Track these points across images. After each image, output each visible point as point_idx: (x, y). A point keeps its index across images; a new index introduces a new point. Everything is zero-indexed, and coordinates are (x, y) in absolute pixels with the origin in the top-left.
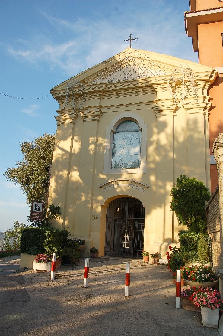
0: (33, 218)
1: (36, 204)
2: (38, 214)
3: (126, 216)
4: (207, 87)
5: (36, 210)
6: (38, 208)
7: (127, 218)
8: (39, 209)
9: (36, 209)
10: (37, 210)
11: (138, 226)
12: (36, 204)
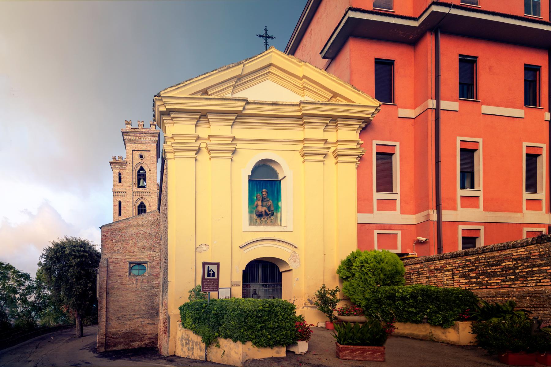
0: (206, 288)
1: (209, 267)
3: (529, 102)
5: (210, 277)
6: (211, 272)
8: (213, 275)
9: (209, 275)
10: (211, 276)
12: (209, 267)
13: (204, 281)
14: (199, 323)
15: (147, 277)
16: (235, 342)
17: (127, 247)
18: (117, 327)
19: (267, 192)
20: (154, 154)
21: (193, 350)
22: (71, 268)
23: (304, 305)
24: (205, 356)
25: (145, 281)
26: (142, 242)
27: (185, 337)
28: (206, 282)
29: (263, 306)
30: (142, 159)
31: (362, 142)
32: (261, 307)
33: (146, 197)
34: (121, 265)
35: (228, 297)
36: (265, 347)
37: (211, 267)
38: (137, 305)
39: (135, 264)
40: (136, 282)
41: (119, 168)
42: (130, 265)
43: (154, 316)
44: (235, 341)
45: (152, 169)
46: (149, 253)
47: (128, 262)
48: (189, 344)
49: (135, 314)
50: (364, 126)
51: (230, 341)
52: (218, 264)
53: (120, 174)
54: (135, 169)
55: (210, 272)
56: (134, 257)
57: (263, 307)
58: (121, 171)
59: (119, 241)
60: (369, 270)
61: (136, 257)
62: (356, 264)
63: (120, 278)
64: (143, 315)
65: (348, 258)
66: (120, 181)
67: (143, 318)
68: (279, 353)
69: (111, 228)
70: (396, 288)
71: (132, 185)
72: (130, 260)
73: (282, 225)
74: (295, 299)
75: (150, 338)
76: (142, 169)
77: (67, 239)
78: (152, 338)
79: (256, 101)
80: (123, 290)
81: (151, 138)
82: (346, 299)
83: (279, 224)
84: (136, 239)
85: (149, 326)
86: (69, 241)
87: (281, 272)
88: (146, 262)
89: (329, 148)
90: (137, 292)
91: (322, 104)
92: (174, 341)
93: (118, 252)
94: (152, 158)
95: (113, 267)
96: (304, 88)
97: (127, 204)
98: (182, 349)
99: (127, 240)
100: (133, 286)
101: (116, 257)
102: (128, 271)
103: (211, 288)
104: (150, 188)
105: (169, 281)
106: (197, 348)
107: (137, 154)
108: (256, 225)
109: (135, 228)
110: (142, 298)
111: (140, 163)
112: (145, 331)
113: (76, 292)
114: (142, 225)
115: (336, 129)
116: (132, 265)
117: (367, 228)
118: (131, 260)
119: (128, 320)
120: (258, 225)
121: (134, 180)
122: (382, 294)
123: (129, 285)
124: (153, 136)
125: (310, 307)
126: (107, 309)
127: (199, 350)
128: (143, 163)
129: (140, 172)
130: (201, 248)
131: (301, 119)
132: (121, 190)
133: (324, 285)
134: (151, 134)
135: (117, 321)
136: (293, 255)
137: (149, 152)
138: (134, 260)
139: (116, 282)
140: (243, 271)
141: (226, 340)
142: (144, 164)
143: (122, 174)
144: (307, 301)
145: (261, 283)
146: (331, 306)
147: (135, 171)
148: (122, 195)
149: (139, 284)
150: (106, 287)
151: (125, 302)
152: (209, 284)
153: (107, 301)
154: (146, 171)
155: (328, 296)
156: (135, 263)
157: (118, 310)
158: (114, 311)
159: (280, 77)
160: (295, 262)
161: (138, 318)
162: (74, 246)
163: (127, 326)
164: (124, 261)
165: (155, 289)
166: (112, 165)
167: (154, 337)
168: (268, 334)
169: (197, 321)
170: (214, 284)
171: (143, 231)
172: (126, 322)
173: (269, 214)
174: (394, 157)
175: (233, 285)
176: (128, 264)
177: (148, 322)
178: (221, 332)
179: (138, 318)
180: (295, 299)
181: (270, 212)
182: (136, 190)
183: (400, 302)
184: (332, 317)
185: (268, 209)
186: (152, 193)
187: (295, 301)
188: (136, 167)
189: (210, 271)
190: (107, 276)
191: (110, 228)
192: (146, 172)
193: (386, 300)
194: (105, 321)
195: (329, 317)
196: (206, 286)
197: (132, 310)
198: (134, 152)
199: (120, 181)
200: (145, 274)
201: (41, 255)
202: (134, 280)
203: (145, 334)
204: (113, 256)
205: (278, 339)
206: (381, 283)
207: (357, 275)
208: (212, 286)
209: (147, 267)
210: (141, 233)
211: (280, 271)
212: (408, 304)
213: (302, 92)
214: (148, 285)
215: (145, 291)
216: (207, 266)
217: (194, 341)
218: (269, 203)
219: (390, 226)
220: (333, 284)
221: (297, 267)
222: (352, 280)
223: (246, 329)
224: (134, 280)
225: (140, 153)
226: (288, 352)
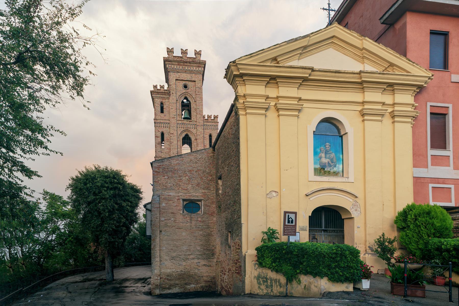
0: (286, 233)
1: (288, 216)
5: (290, 223)
7: (323, 228)
8: (292, 222)
9: (289, 222)
12: (288, 216)
13: (285, 227)
14: (279, 262)
15: (202, 215)
16: (315, 278)
17: (180, 184)
18: (172, 267)
19: (330, 146)
21: (272, 288)
22: (103, 201)
23: (364, 252)
24: (286, 292)
25: (199, 219)
26: (195, 179)
27: (262, 275)
28: (287, 228)
29: (336, 249)
30: (186, 89)
31: (417, 105)
32: (335, 251)
33: (191, 130)
34: (174, 202)
35: (297, 241)
36: (337, 282)
38: (192, 244)
39: (188, 202)
40: (191, 220)
42: (183, 203)
43: (210, 257)
44: (314, 277)
45: (198, 100)
46: (203, 191)
48: (267, 282)
49: (190, 255)
50: (419, 91)
51: (310, 277)
52: (295, 213)
57: (337, 251)
58: (164, 101)
59: (172, 177)
60: (422, 224)
61: (190, 195)
62: (413, 213)
63: (173, 216)
64: (199, 256)
65: (404, 209)
66: (162, 111)
67: (198, 259)
68: (348, 288)
69: (163, 164)
70: (443, 240)
71: (176, 116)
72: (183, 198)
73: (344, 176)
75: (206, 281)
77: (96, 168)
78: (209, 281)
79: (321, 69)
80: (177, 228)
81: (196, 68)
82: (402, 248)
83: (342, 175)
85: (204, 267)
86: (99, 171)
87: (343, 219)
88: (200, 201)
89: (387, 110)
90: (192, 231)
91: (379, 74)
93: (171, 189)
95: (166, 203)
96: (364, 57)
98: (259, 287)
100: (188, 224)
101: (168, 194)
102: (182, 208)
103: (291, 233)
104: (196, 120)
106: (277, 285)
107: (181, 84)
108: (320, 175)
109: (188, 165)
110: (197, 238)
111: (185, 93)
112: (201, 272)
113: (108, 228)
114: (196, 163)
115: (393, 92)
117: (423, 181)
118: (185, 198)
119: (183, 260)
120: (322, 175)
122: (431, 246)
123: (183, 223)
124: (199, 67)
125: (371, 254)
127: (279, 287)
128: (188, 94)
131: (361, 84)
132: (164, 121)
133: (383, 233)
134: (196, 64)
135: (172, 261)
137: (194, 83)
138: (188, 198)
140: (309, 216)
141: (306, 276)
142: (189, 94)
143: (164, 104)
144: (368, 248)
146: (390, 254)
149: (194, 223)
150: (159, 224)
151: (179, 241)
154: (191, 102)
155: (387, 244)
156: (189, 200)
157: (172, 249)
158: (168, 250)
159: (342, 46)
161: (193, 259)
162: (106, 177)
163: (183, 267)
164: (177, 199)
165: (211, 228)
166: (153, 94)
167: (210, 280)
168: (340, 272)
169: (278, 260)
170: (293, 229)
171: (196, 168)
174: (447, 116)
176: (182, 202)
177: (204, 263)
178: (302, 269)
179: (193, 259)
180: (357, 245)
182: (180, 122)
183: (446, 253)
184: (391, 264)
185: (331, 161)
186: (198, 126)
189: (290, 219)
191: (161, 164)
192: (190, 103)
193: (435, 251)
194: (159, 260)
195: (388, 264)
196: (287, 231)
197: (187, 249)
198: (177, 81)
199: (162, 111)
200: (199, 213)
201: (67, 186)
202: (188, 218)
203: (201, 276)
204: (166, 193)
206: (432, 236)
207: (411, 226)
209: (202, 205)
211: (342, 218)
212: (452, 255)
213: (362, 60)
214: (203, 224)
215: (200, 231)
216: (287, 214)
217: (273, 279)
218: (332, 156)
219: (444, 181)
220: (392, 234)
222: (408, 230)
223: (323, 267)
224: (188, 218)
225: (184, 82)
226: (354, 288)
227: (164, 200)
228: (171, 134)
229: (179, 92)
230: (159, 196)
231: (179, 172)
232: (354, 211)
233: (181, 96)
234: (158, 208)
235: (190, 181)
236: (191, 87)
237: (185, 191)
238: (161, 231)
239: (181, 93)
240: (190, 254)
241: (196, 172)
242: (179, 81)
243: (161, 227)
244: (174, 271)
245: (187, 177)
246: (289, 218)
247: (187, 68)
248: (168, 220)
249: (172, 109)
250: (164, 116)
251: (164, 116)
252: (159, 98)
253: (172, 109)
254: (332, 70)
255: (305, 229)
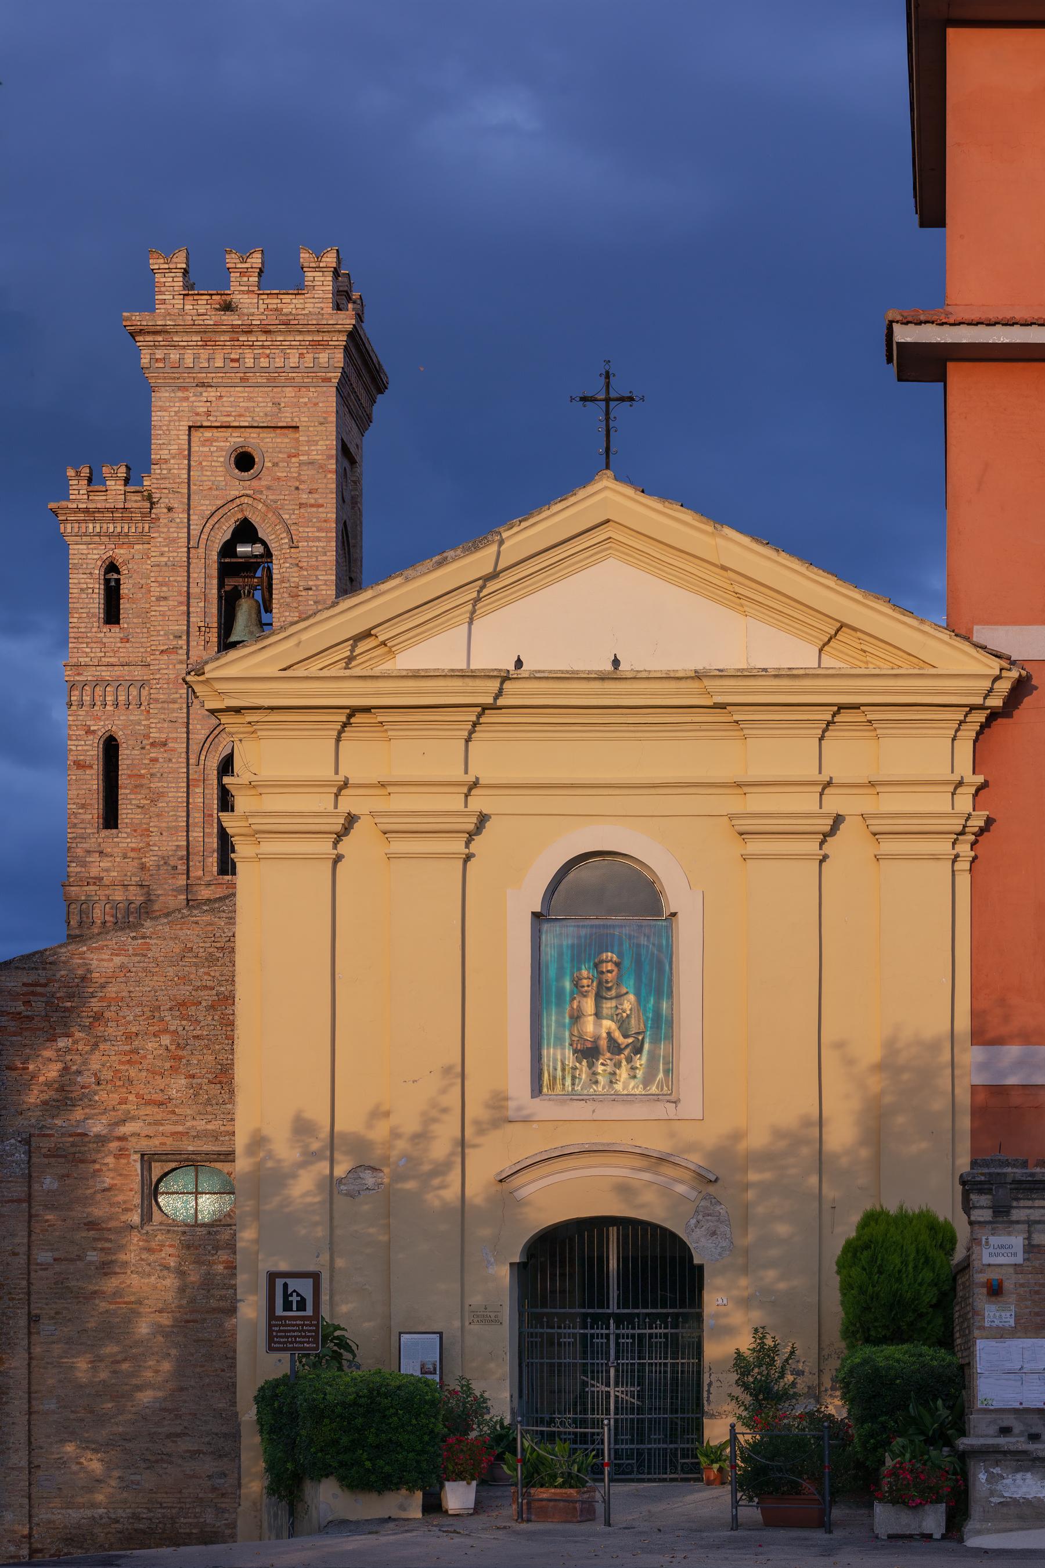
1: (285, 1286)
2: (298, 1325)
4: (969, 733)
5: (292, 1310)
6: (294, 1299)
7: (613, 1308)
8: (302, 1305)
9: (287, 1306)
11: (633, 1344)
12: (285, 1286)
17: (133, 1072)
20: (322, 446)
26: (207, 1046)
28: (280, 1326)
35: (431, 1367)
37: (293, 1284)
39: (173, 1165)
41: (105, 539)
45: (307, 539)
47: (138, 1157)
49: (178, 1435)
53: (112, 567)
54: (202, 545)
55: (290, 1299)
56: (169, 1128)
58: (121, 554)
61: (180, 1129)
71: (182, 642)
72: (144, 1145)
74: (713, 1378)
76: (245, 531)
79: (539, 671)
81: (301, 356)
84: (176, 1032)
92: (256, 1517)
94: (307, 472)
97: (154, 760)
99: (129, 1037)
102: (137, 1201)
103: (296, 1342)
105: (240, 1300)
109: (171, 971)
116: (157, 1170)
119: (143, 1465)
121: (197, 606)
124: (316, 345)
126: (34, 1403)
128: (255, 504)
129: (234, 554)
130: (355, 1179)
132: (118, 671)
136: (706, 1208)
137: (291, 434)
138: (170, 1144)
139: (80, 1258)
143: (124, 570)
145: (618, 1308)
147: (201, 550)
148: (122, 698)
150: (24, 1283)
152: (290, 1331)
153: (30, 1358)
154: (273, 546)
156: (178, 1157)
160: (714, 1233)
161: (194, 1454)
170: (305, 1331)
172: (133, 1477)
173: (623, 1046)
175: (476, 1320)
176: (138, 1166)
179: (194, 1454)
180: (713, 1378)
181: (630, 1040)
185: (619, 1028)
187: (715, 1384)
188: (207, 530)
189: (291, 1295)
190: (29, 1227)
192: (268, 554)
194: (24, 1463)
196: (281, 1337)
202: (171, 1251)
205: (387, 1469)
208: (299, 1337)
210: (204, 1004)
216: (279, 1283)
221: (720, 1254)
227: (52, 1160)
228: (152, 745)
229: (205, 497)
230: (27, 1142)
231: (125, 1011)
232: (703, 1240)
233: (215, 519)
234: (19, 1201)
235: (181, 1058)
236: (275, 464)
237: (156, 1109)
238: (33, 1319)
239: (220, 503)
240: (178, 1430)
241: (212, 1007)
242: (208, 434)
243: (33, 1297)
244: (101, 1518)
245: (166, 1040)
246: (289, 1292)
247: (249, 362)
248: (72, 1260)
249: (165, 598)
250: (122, 640)
251: (122, 640)
252: (97, 539)
253: (165, 598)
254: (583, 672)
255: (493, 1315)
